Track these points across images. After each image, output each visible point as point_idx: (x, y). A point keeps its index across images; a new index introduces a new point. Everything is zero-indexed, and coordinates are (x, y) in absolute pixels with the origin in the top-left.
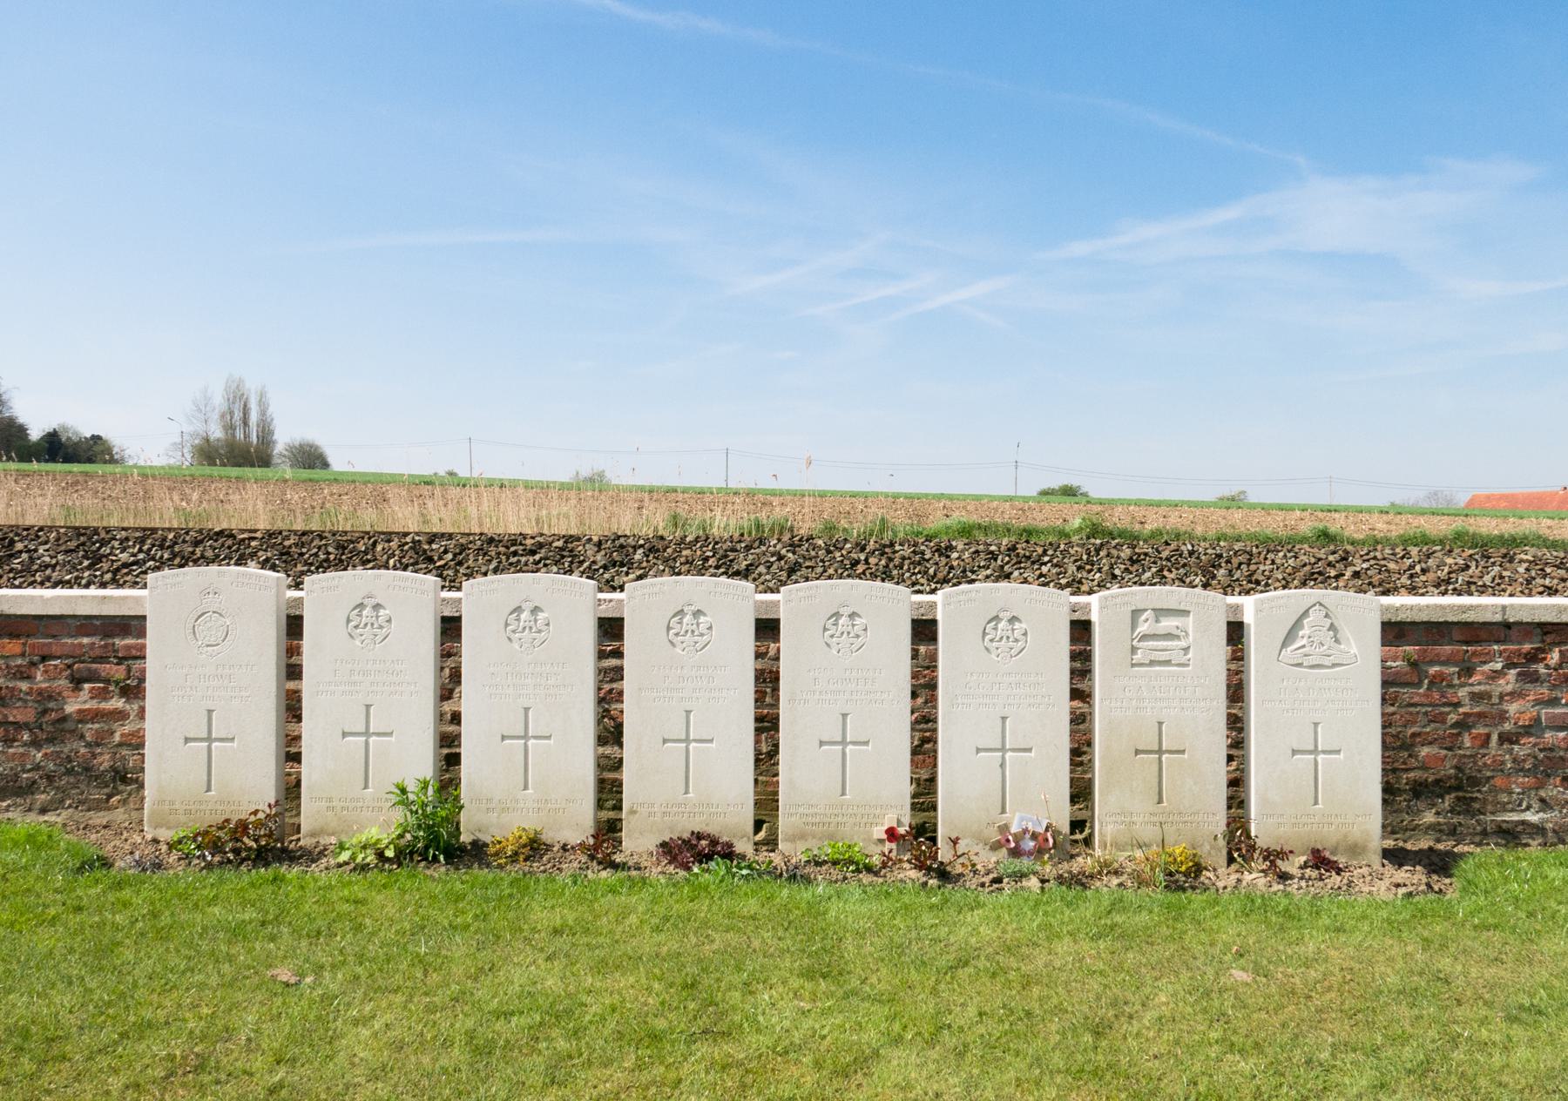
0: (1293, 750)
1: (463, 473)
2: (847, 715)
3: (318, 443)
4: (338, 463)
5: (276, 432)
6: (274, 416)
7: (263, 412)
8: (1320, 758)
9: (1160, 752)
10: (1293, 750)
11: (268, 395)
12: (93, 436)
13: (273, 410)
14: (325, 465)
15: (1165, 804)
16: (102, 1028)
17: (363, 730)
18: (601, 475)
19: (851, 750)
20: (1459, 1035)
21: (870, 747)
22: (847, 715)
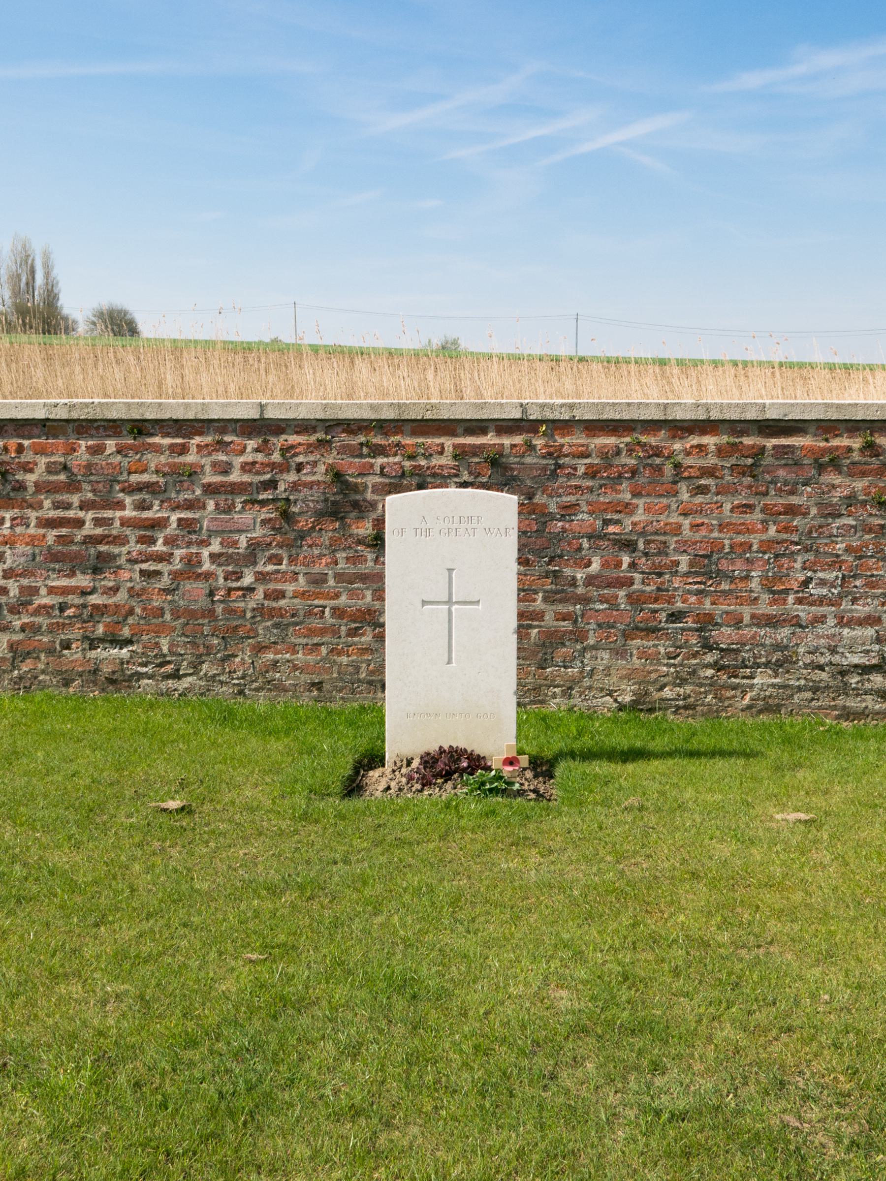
0: (423, 601)
1: (288, 338)
2: (453, 569)
3: (95, 305)
4: (146, 329)
5: (61, 296)
6: (58, 278)
7: (47, 275)
8: (454, 608)
9: (449, 602)
10: (423, 601)
11: (52, 256)
12: (275, 341)
13: (58, 272)
14: (133, 331)
15: (454, 665)
16: (148, 915)
17: (446, 599)
18: (455, 342)
19: (456, 609)
20: (13, 1114)
21: (480, 607)
22: (453, 569)
